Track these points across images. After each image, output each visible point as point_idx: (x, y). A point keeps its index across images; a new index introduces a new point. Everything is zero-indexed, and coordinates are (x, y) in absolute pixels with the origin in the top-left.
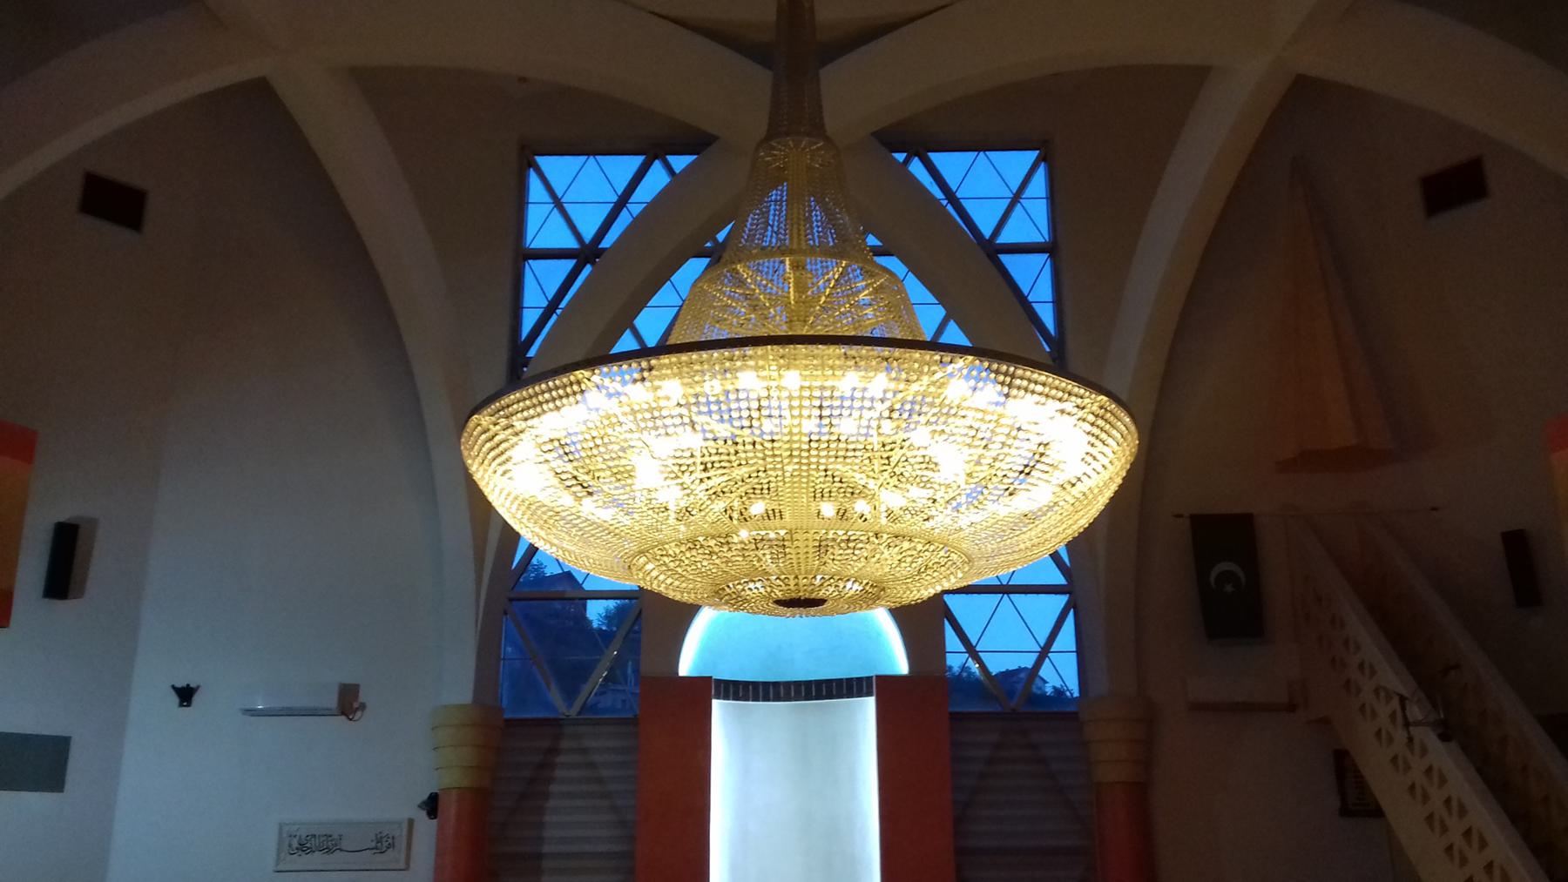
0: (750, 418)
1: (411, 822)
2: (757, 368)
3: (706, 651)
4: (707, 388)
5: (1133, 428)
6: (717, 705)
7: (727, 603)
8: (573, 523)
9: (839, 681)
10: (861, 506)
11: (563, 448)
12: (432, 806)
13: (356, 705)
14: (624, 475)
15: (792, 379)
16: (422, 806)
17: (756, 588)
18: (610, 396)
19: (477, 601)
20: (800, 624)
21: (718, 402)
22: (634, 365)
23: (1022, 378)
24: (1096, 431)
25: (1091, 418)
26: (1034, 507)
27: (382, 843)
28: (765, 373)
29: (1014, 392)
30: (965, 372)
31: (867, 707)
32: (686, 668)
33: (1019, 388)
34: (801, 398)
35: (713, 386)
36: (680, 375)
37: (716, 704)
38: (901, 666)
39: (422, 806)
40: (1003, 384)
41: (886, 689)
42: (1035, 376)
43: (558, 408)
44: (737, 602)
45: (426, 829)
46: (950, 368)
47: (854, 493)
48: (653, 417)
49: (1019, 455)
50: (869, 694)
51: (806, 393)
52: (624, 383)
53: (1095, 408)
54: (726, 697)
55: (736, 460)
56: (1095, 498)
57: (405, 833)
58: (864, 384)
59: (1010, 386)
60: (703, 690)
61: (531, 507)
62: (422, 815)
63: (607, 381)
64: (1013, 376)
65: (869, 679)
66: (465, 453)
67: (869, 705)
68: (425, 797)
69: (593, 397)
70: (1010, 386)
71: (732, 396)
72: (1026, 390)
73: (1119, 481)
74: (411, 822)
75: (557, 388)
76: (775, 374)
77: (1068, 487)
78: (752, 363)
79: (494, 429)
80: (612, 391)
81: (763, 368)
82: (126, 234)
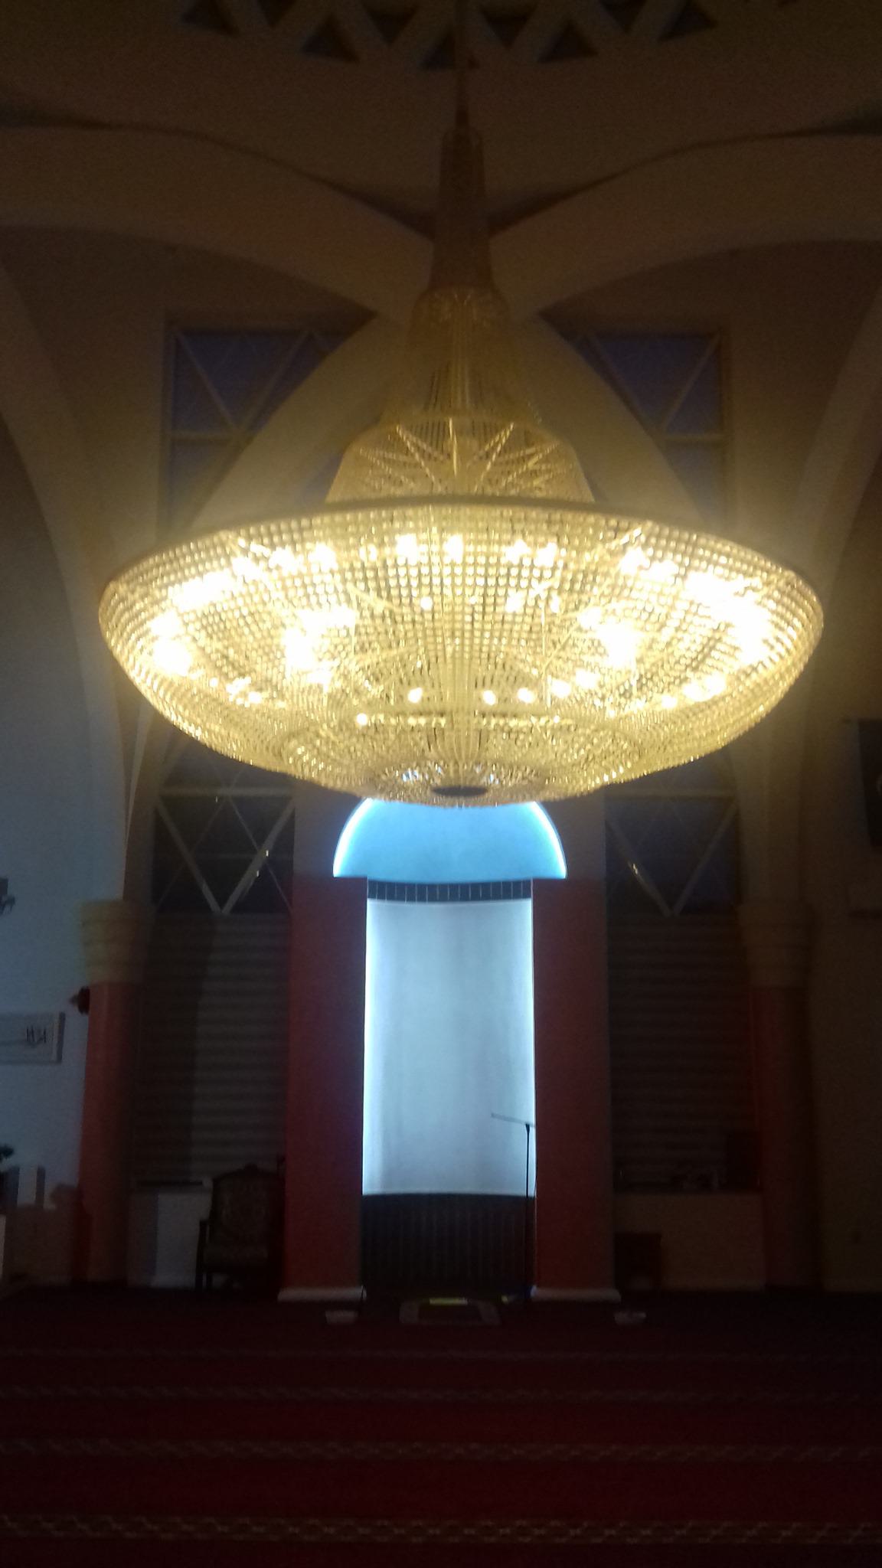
1: (62, 1017)
2: (416, 530)
3: (360, 849)
4: (363, 555)
5: (819, 609)
6: (371, 905)
7: (382, 790)
8: (217, 706)
10: (525, 696)
11: (213, 623)
12: (83, 1001)
13: (4, 899)
14: (272, 653)
15: (456, 545)
17: (412, 777)
18: (257, 559)
19: (128, 801)
20: (458, 816)
21: (375, 570)
22: (283, 526)
23: (704, 548)
24: (780, 609)
25: (776, 594)
26: (706, 697)
27: (34, 1036)
29: (696, 563)
30: (643, 539)
31: (525, 910)
33: (701, 559)
35: (369, 553)
36: (334, 537)
38: (560, 870)
39: (73, 1000)
41: (544, 892)
42: (719, 546)
43: (200, 574)
44: (391, 790)
45: (78, 1025)
46: (625, 538)
47: (520, 680)
48: (305, 589)
49: (687, 646)
50: (526, 896)
53: (782, 584)
55: (395, 629)
56: (776, 684)
58: (534, 554)
59: (692, 556)
61: (180, 692)
64: (695, 546)
66: (103, 626)
67: (527, 907)
68: (76, 991)
69: (240, 563)
70: (692, 556)
73: (801, 666)
74: (62, 1017)
76: (436, 536)
77: (743, 677)
82: (10, 884)
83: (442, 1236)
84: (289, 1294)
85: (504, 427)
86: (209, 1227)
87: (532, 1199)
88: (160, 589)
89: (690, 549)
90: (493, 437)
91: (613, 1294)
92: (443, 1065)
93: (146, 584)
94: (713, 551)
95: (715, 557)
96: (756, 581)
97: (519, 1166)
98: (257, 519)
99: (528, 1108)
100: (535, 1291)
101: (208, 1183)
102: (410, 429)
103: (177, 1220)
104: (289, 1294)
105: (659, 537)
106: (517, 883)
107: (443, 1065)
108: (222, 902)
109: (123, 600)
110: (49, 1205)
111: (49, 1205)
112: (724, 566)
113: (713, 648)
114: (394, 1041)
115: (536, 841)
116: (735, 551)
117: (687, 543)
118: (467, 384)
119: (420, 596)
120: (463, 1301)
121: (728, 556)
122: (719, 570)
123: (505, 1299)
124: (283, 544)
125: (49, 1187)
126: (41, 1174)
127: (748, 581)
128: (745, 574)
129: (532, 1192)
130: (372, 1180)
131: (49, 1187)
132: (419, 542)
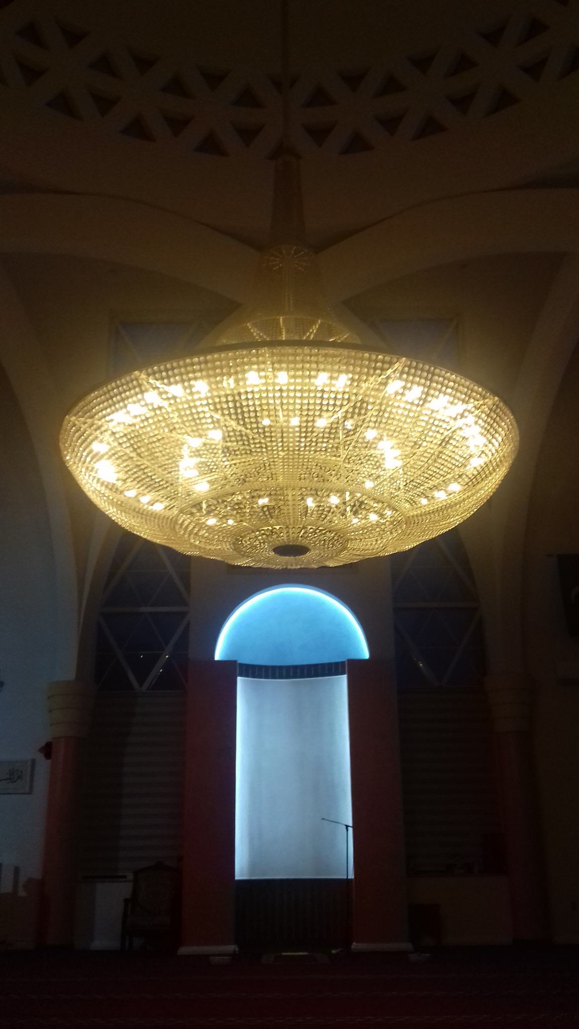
0: (255, 411)
1: (33, 762)
3: (232, 645)
9: (323, 665)
12: (47, 750)
16: (41, 750)
28: (262, 374)
31: (342, 682)
32: (219, 654)
33: (435, 389)
34: (288, 390)
35: (229, 383)
37: (240, 680)
38: (365, 653)
39: (41, 750)
40: (424, 385)
45: (43, 766)
51: (292, 388)
52: (170, 384)
54: (247, 676)
55: (248, 430)
57: (29, 770)
58: (332, 381)
60: (230, 670)
62: (40, 757)
63: (158, 383)
64: (433, 374)
65: (343, 663)
68: (43, 744)
70: (431, 381)
71: (243, 397)
72: (440, 391)
75: (122, 385)
76: (270, 374)
78: (255, 367)
79: (84, 427)
80: (161, 390)
81: (263, 370)
83: (290, 907)
84: (184, 950)
85: (314, 323)
86: (131, 903)
87: (351, 880)
88: (99, 420)
89: (430, 376)
90: (308, 331)
91: (407, 946)
92: (289, 787)
93: (92, 417)
94: (445, 378)
95: (446, 382)
96: (470, 406)
97: (341, 857)
98: (158, 362)
99: (348, 818)
100: (354, 945)
101: (130, 876)
102: (255, 325)
103: (109, 901)
104: (184, 950)
105: (410, 367)
106: (337, 664)
107: (289, 787)
108: (141, 685)
109: (74, 425)
110: (22, 893)
111: (22, 893)
112: (450, 395)
113: (448, 442)
114: (256, 772)
115: (349, 636)
116: (458, 379)
117: (428, 372)
118: (292, 302)
119: (262, 417)
120: (306, 953)
121: (454, 382)
122: (447, 397)
123: (334, 952)
124: (176, 383)
125: (22, 879)
126: (17, 870)
127: (465, 406)
128: (463, 401)
129: (351, 876)
130: (242, 868)
131: (22, 879)
132: (261, 377)
